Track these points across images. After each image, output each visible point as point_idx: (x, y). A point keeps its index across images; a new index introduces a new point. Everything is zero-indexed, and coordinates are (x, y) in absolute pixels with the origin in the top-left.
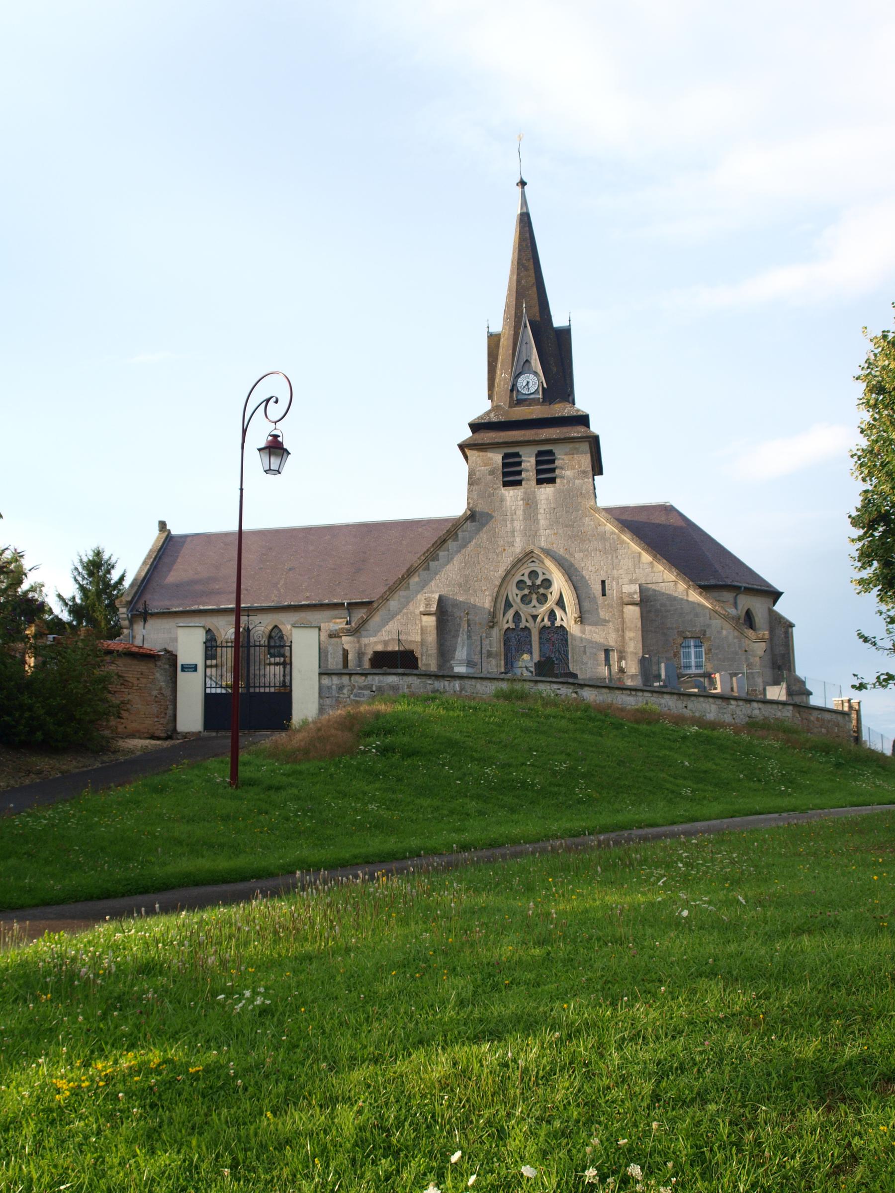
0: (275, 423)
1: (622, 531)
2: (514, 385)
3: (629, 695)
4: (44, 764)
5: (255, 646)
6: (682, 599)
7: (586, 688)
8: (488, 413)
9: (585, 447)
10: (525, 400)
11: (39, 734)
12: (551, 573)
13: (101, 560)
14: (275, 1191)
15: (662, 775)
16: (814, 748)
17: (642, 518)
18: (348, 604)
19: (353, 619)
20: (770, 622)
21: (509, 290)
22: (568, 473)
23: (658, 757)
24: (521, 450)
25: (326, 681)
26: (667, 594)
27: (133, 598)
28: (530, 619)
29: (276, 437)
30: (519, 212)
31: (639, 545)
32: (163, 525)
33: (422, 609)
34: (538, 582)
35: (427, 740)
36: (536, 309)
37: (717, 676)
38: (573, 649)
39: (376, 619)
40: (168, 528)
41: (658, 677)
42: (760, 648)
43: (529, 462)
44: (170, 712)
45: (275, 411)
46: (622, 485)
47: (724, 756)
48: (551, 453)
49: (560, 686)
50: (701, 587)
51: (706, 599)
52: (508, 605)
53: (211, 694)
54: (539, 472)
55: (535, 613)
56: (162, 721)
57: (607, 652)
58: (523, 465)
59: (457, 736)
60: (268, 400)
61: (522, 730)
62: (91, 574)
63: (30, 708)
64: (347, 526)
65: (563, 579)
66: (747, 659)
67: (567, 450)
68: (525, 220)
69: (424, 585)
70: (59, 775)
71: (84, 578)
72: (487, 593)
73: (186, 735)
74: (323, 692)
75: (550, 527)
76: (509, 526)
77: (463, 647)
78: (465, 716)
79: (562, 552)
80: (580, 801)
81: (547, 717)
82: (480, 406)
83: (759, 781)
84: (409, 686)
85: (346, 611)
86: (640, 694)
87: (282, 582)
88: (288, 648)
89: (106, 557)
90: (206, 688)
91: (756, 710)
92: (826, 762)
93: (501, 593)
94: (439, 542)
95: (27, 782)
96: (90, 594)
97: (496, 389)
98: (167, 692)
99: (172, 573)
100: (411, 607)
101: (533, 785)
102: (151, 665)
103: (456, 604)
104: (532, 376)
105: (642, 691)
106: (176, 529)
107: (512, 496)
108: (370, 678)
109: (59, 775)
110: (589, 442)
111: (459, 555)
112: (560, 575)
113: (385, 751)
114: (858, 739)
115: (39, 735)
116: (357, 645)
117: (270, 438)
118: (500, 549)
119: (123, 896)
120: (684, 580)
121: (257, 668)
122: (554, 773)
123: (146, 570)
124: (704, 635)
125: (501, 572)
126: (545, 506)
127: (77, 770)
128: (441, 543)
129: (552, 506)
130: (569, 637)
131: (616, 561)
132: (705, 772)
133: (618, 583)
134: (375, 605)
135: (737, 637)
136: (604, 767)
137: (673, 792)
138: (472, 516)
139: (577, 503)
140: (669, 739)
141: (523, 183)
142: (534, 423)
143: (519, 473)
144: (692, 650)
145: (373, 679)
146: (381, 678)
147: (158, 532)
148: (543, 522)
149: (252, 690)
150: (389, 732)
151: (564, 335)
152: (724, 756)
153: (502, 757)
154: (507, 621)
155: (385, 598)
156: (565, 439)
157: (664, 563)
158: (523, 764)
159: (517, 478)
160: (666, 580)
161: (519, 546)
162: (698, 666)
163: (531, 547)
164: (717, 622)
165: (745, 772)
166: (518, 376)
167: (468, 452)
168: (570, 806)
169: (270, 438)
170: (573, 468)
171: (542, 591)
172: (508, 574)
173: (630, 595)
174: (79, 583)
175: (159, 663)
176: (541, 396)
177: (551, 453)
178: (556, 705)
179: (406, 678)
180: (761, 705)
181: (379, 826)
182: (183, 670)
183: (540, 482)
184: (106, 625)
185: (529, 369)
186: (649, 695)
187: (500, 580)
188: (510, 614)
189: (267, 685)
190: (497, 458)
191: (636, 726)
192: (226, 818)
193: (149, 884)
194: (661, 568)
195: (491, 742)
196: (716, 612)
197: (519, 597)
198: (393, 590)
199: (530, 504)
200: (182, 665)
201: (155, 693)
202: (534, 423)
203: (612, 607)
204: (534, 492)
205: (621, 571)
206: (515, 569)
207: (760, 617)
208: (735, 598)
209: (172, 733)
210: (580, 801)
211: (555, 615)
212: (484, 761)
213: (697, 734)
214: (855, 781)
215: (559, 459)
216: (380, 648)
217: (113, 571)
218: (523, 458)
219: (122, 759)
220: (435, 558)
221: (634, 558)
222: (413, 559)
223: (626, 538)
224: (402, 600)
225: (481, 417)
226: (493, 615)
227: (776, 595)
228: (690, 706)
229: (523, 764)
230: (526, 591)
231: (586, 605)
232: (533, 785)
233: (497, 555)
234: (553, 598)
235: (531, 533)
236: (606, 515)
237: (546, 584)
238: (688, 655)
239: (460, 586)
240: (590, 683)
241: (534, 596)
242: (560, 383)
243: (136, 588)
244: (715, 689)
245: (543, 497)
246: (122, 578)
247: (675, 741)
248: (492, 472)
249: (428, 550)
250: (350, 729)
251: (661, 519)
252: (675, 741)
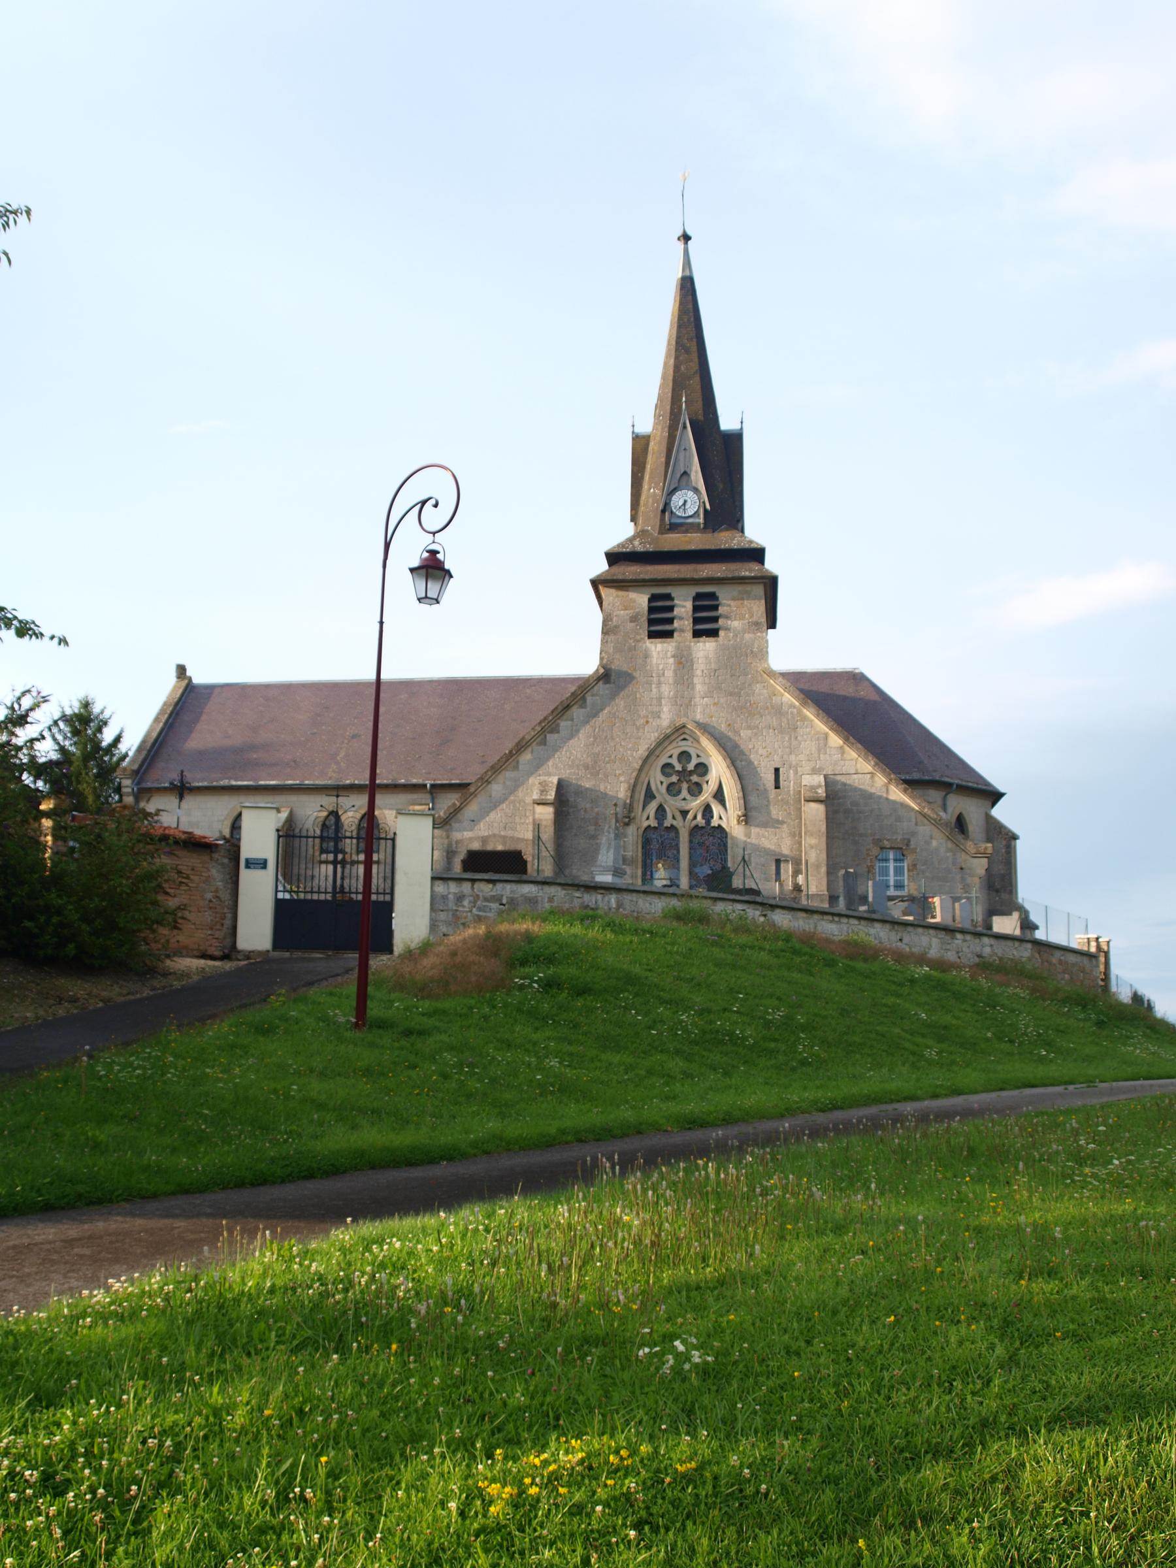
0: (434, 533)
1: (804, 704)
2: (667, 505)
3: (831, 922)
4: (77, 987)
6: (880, 797)
7: (778, 911)
9: (759, 590)
10: (681, 525)
11: (71, 946)
12: (709, 756)
13: (90, 713)
14: (6, 1515)
15: (897, 1030)
16: (1066, 1000)
17: (824, 688)
18: (432, 786)
19: (437, 806)
21: (664, 377)
22: (735, 624)
23: (885, 1005)
25: (440, 888)
26: (861, 790)
27: (141, 766)
29: (433, 553)
30: (680, 275)
31: (826, 723)
32: (181, 670)
33: (536, 796)
34: (691, 767)
35: (599, 973)
36: (699, 405)
37: (937, 900)
38: (733, 857)
39: (472, 808)
40: (188, 674)
41: (864, 899)
42: (980, 866)
43: (684, 607)
44: (228, 922)
45: (434, 518)
46: (798, 644)
47: (963, 1007)
48: (668, 597)
49: (744, 906)
50: (906, 782)
51: (912, 797)
52: (650, 796)
53: (284, 900)
54: (696, 621)
55: (687, 808)
56: (218, 934)
57: (778, 862)
58: (676, 611)
59: (637, 970)
60: (424, 503)
61: (716, 965)
62: (76, 732)
63: (59, 911)
64: (431, 682)
65: (724, 765)
66: (963, 879)
67: (735, 593)
68: (687, 287)
69: (538, 765)
70: (101, 1005)
71: (65, 738)
72: (622, 779)
73: (248, 955)
74: (436, 903)
75: (708, 694)
76: (654, 690)
77: (608, 849)
78: (641, 943)
79: (723, 728)
80: (804, 1063)
81: (743, 947)
83: (1011, 1041)
84: (551, 900)
85: (428, 796)
86: (844, 920)
87: (342, 754)
88: (389, 842)
89: (96, 709)
90: (277, 891)
91: (986, 947)
92: (1085, 1020)
93: (641, 779)
94: (560, 708)
95: (61, 1012)
96: (74, 758)
97: (642, 509)
98: (226, 896)
99: (193, 735)
100: (520, 793)
101: (745, 1039)
102: (206, 858)
103: (580, 792)
104: (691, 493)
105: (848, 916)
106: (199, 677)
107: (659, 650)
108: (499, 886)
109: (101, 1005)
110: (765, 584)
111: (588, 727)
112: (720, 758)
113: (549, 985)
114: (1106, 987)
115: (71, 949)
116: (446, 841)
117: (426, 555)
118: (642, 721)
119: (283, 1182)
120: (883, 772)
121: (303, 866)
122: (767, 1024)
123: (158, 730)
124: (908, 845)
125: (642, 751)
126: (702, 667)
127: (123, 999)
128: (564, 709)
129: (713, 666)
130: (729, 841)
131: (794, 743)
132: (945, 1027)
133: (796, 773)
134: (472, 789)
135: (949, 850)
136: (825, 1017)
137: (913, 1053)
138: (606, 675)
139: (745, 663)
140: (894, 983)
141: (686, 238)
142: (691, 558)
143: (670, 621)
144: (891, 865)
145: (503, 889)
146: (514, 886)
147: (175, 679)
148: (699, 688)
149: (374, 897)
150: (550, 960)
151: (734, 441)
152: (963, 1007)
153: (698, 999)
154: (647, 817)
155: (485, 780)
156: (733, 578)
157: (858, 749)
158: (725, 1010)
159: (667, 627)
160: (860, 770)
161: (666, 718)
162: (899, 886)
163: (683, 720)
164: (925, 829)
165: (992, 1029)
166: (672, 493)
167: (604, 591)
168: (794, 1069)
169: (426, 555)
170: (742, 618)
171: (695, 778)
172: (651, 754)
173: (813, 788)
174: (58, 744)
175: (216, 856)
176: (701, 520)
178: (748, 931)
179: (547, 889)
180: (993, 941)
181: (566, 1090)
182: (247, 867)
183: (697, 634)
184: (94, 801)
185: (687, 484)
186: (856, 922)
187: (640, 763)
188: (652, 807)
189: (315, 889)
190: (641, 600)
191: (851, 963)
192: (367, 1072)
193: (315, 1165)
194: (854, 755)
195: (679, 978)
196: (924, 816)
197: (665, 785)
198: (496, 769)
199: (684, 662)
200: (247, 860)
201: (209, 896)
202: (691, 558)
203: (787, 803)
204: (690, 647)
205: (801, 757)
206: (660, 749)
207: (975, 823)
208: (945, 798)
209: (230, 952)
210: (804, 1063)
211: (711, 811)
212: (677, 1004)
213: (927, 978)
214: (1124, 1045)
215: (724, 605)
216: (476, 846)
217: (105, 730)
218: (676, 602)
219: (177, 984)
220: (555, 729)
221: (818, 739)
222: (525, 730)
223: (809, 713)
224: (508, 783)
225: (622, 545)
226: (630, 808)
227: (995, 796)
229: (725, 1010)
230: (674, 779)
231: (753, 800)
232: (745, 1039)
233: (638, 729)
234: (709, 789)
235: (684, 701)
236: (784, 682)
237: (701, 770)
238: (885, 872)
239: (587, 767)
240: (784, 904)
241: (685, 786)
242: (726, 505)
243: (145, 753)
244: (934, 917)
245: (701, 654)
246: (118, 740)
247: (901, 985)
248: (634, 619)
249: (545, 719)
250: (496, 954)
251: (848, 690)
252: (901, 985)
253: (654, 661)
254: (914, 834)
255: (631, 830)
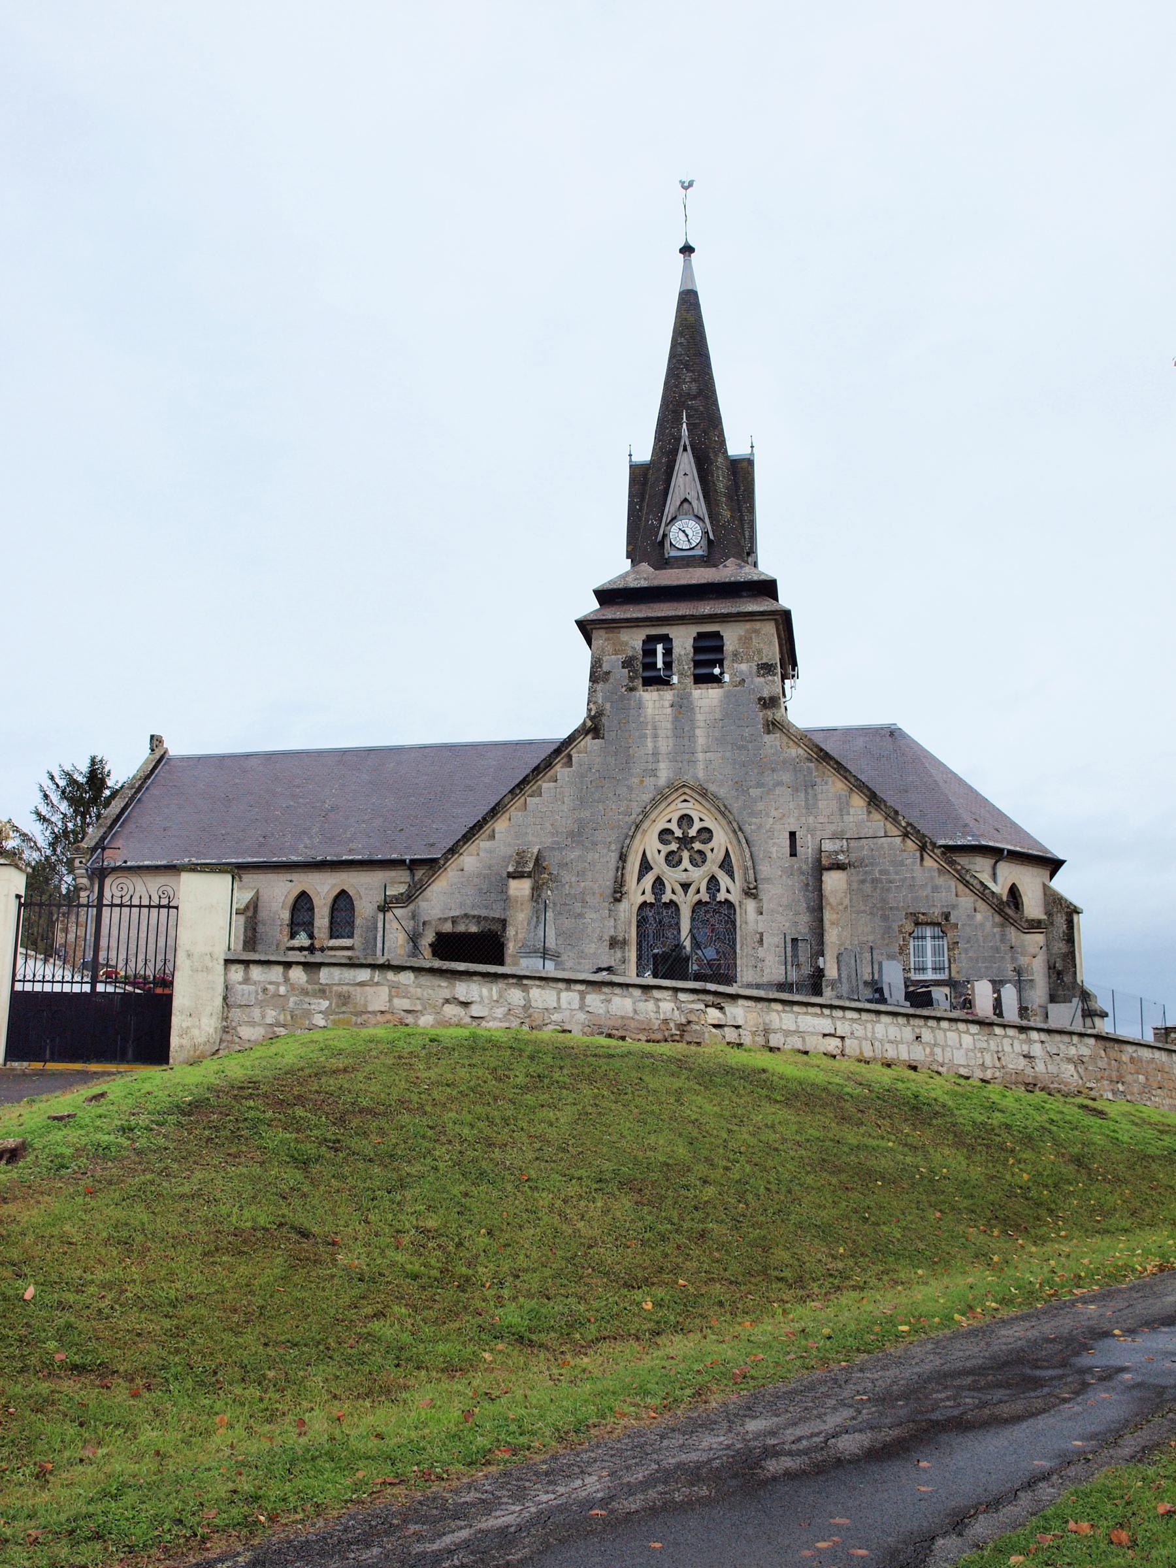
5: (112, 905)
7: (741, 1002)
8: (623, 577)
9: (769, 629)
20: (1046, 904)
24: (674, 632)
28: (679, 889)
33: (511, 869)
34: (692, 832)
43: (683, 640)
53: (24, 993)
68: (689, 302)
76: (650, 745)
82: (614, 564)
90: (14, 981)
106: (175, 748)
107: (654, 702)
128: (542, 768)
138: (593, 727)
142: (691, 583)
148: (701, 741)
151: (742, 470)
154: (638, 892)
177: (717, 636)
183: (700, 680)
188: (649, 879)
197: (663, 854)
199: (682, 707)
202: (691, 583)
216: (447, 928)
227: (1054, 865)
228: (927, 1035)
230: (674, 846)
237: (705, 835)
238: (920, 952)
241: (686, 855)
253: (650, 711)
254: (954, 907)
255: (624, 906)
